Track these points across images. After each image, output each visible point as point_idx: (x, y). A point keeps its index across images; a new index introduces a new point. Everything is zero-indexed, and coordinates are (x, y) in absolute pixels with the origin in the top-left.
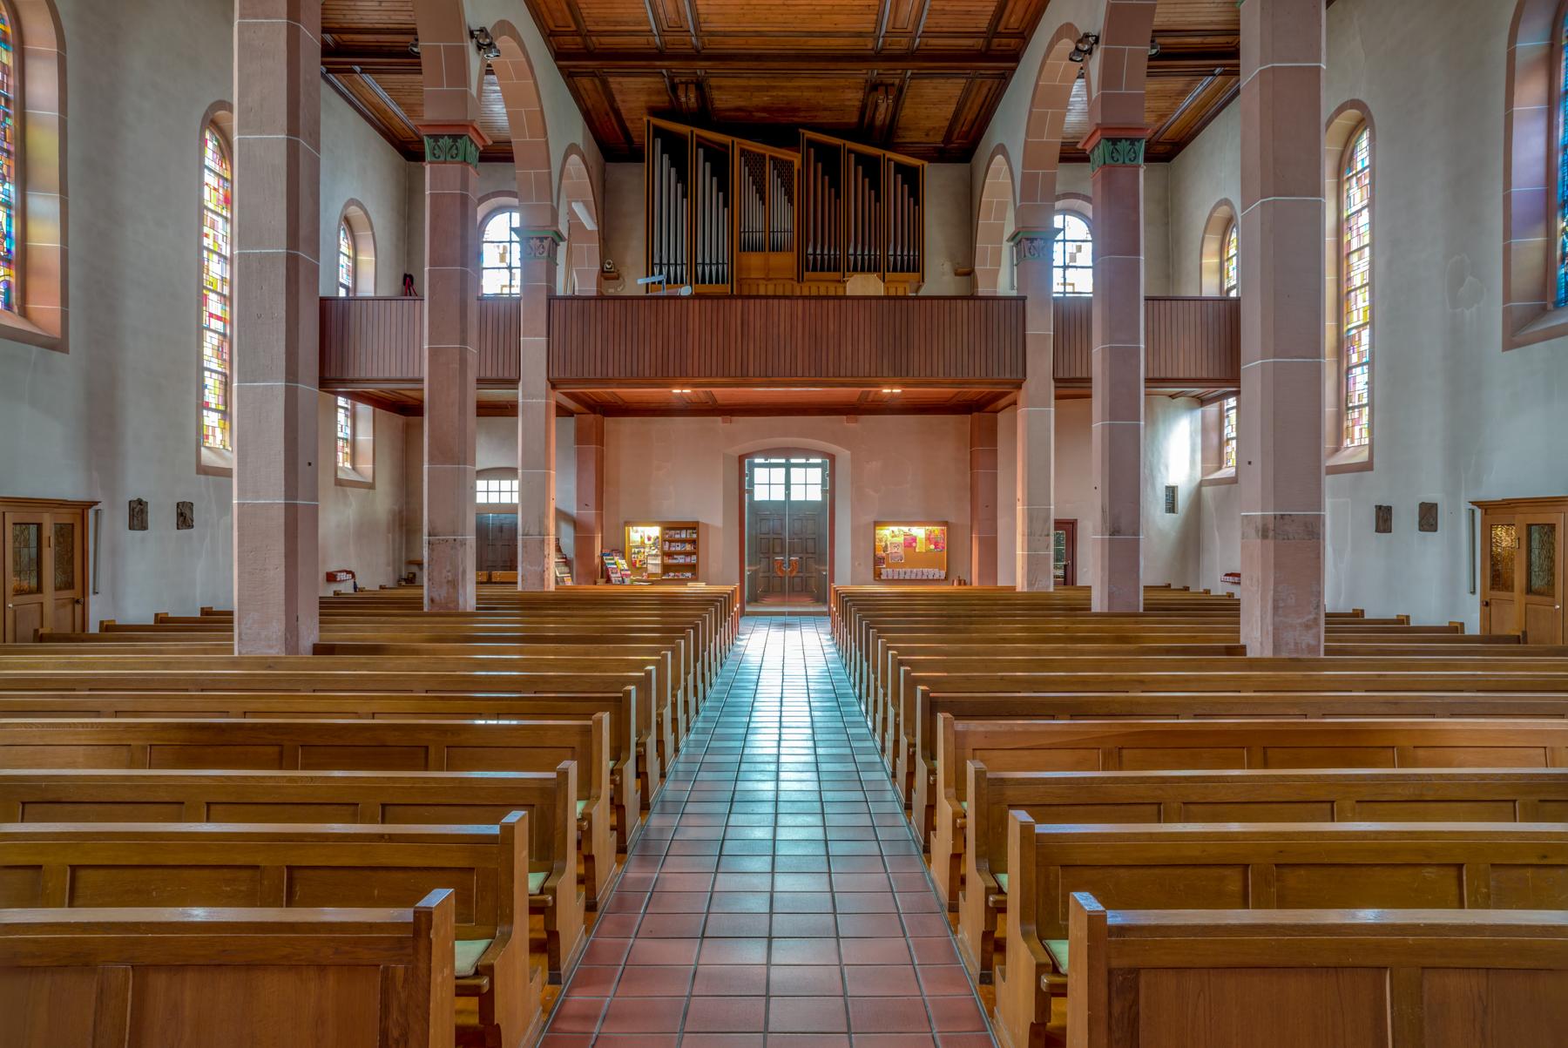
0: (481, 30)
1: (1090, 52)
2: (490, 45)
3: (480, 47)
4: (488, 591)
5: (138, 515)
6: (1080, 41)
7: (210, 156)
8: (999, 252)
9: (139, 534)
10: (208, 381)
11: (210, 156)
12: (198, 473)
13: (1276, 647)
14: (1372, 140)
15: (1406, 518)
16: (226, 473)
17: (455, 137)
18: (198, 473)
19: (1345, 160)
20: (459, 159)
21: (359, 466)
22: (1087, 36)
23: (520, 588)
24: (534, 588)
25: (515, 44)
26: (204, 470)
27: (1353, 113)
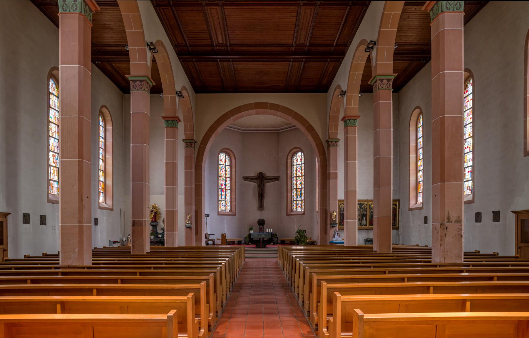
0: (151, 43)
1: (372, 48)
2: (154, 48)
3: (150, 49)
4: (153, 247)
5: (26, 218)
6: (369, 44)
7: (100, 119)
8: (337, 126)
9: (44, 226)
10: (52, 171)
11: (100, 119)
12: (48, 202)
13: (163, 194)
14: (473, 85)
15: (35, 219)
16: (57, 202)
17: (173, 121)
18: (48, 202)
19: (417, 122)
20: (143, 89)
21: (107, 202)
22: (371, 42)
23: (165, 246)
24: (170, 246)
25: (163, 49)
26: (50, 201)
27: (417, 111)
